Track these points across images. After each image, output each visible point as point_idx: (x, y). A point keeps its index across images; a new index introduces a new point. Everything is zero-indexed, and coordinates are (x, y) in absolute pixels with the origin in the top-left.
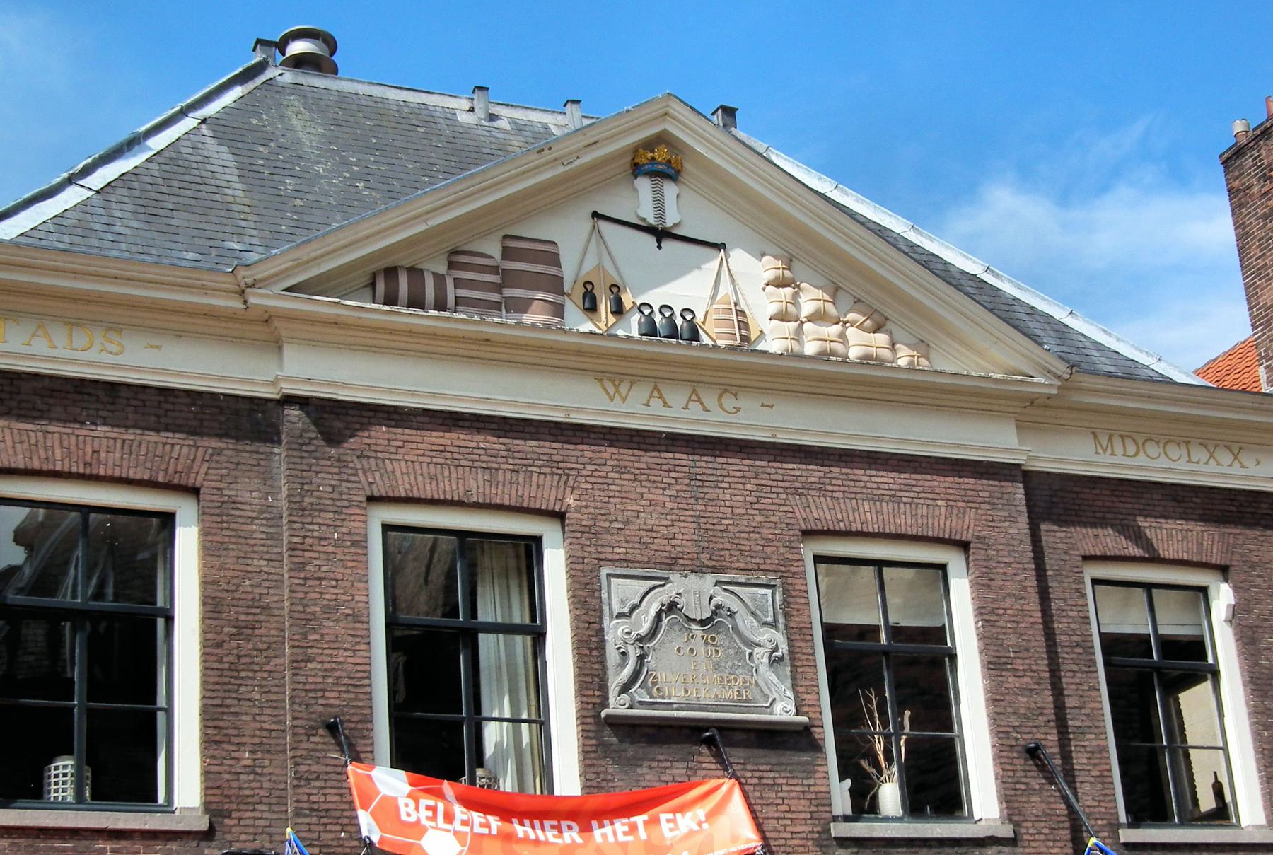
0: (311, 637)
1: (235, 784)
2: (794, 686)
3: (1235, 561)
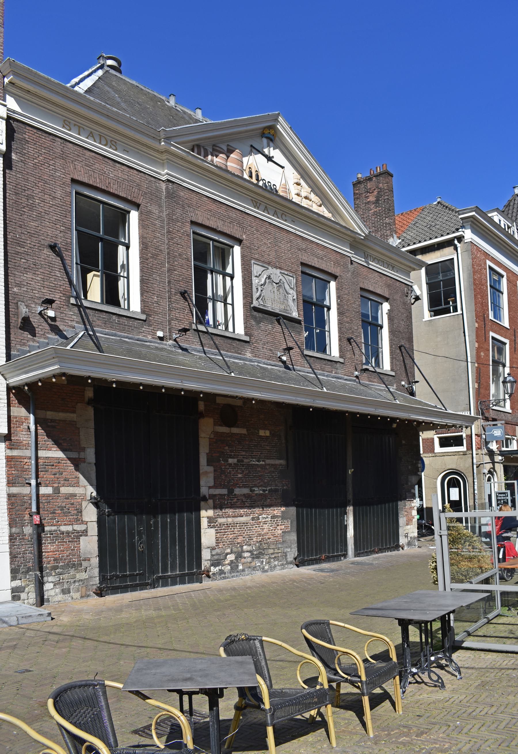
0: (176, 263)
1: (152, 306)
2: (297, 308)
3: (391, 298)
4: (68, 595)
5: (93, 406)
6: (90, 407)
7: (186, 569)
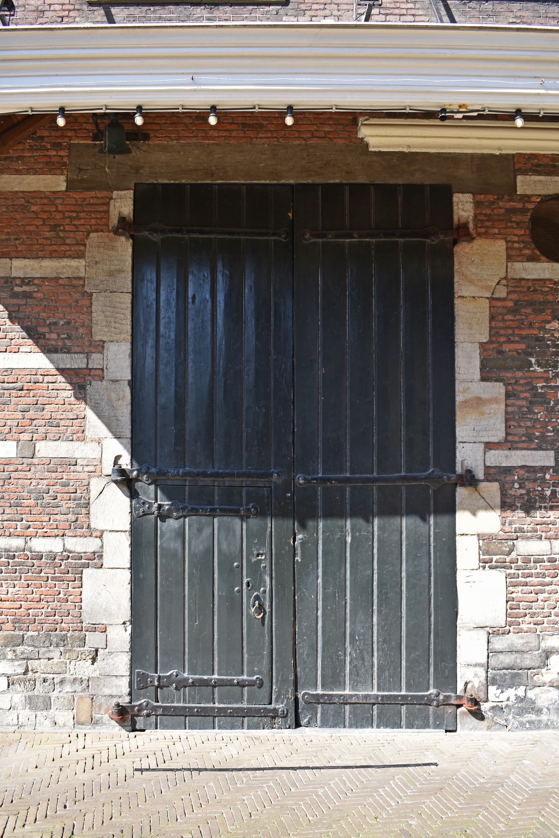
4: (45, 713)
5: (132, 237)
6: (123, 239)
7: (348, 687)
